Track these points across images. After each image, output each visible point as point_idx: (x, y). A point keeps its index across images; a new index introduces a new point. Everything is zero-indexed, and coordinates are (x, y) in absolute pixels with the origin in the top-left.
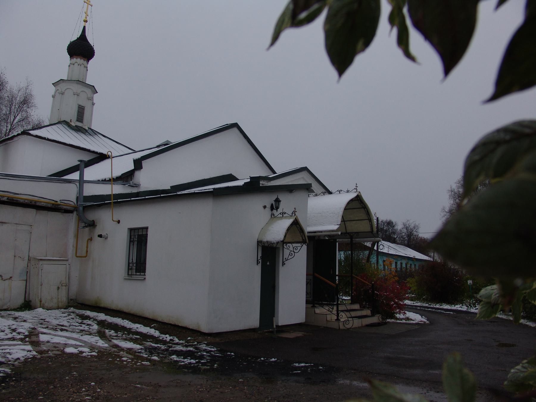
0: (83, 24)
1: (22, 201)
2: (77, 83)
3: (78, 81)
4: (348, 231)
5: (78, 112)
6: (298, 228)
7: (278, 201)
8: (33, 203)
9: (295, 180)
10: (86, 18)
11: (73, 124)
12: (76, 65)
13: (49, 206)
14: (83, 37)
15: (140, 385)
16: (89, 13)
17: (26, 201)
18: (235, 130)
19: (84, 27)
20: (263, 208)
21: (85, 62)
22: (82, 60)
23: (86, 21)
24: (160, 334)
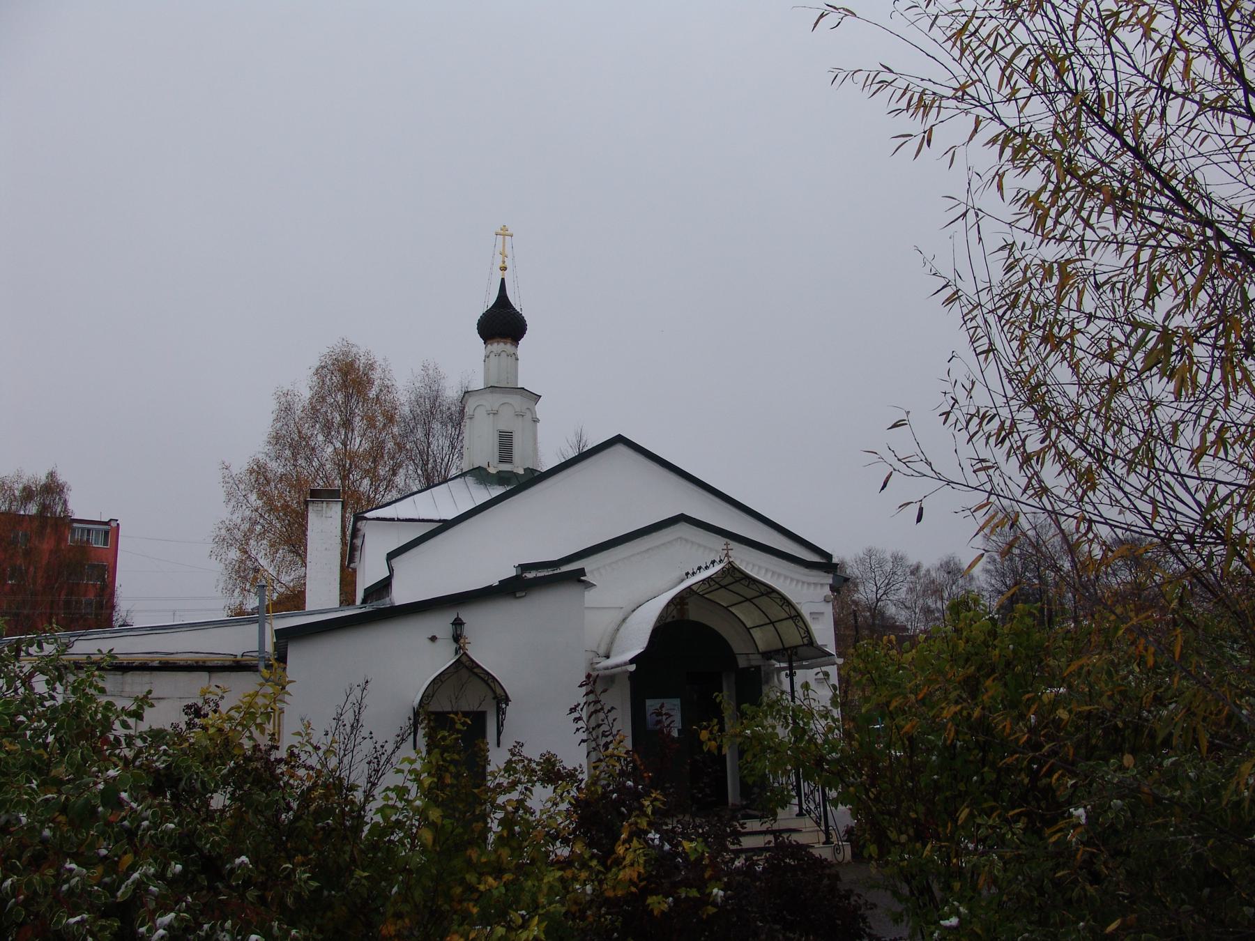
0: (498, 276)
1: (182, 663)
2: (492, 392)
3: (491, 387)
4: (786, 646)
5: (501, 444)
6: (801, 630)
7: (458, 623)
8: (201, 663)
9: (648, 549)
10: (504, 262)
11: (492, 470)
12: (492, 355)
13: (227, 663)
14: (503, 300)
15: (1111, 933)
16: (508, 251)
17: (189, 662)
18: (620, 449)
19: (503, 280)
20: (428, 642)
21: (509, 347)
22: (502, 345)
23: (504, 269)
24: (565, 875)
